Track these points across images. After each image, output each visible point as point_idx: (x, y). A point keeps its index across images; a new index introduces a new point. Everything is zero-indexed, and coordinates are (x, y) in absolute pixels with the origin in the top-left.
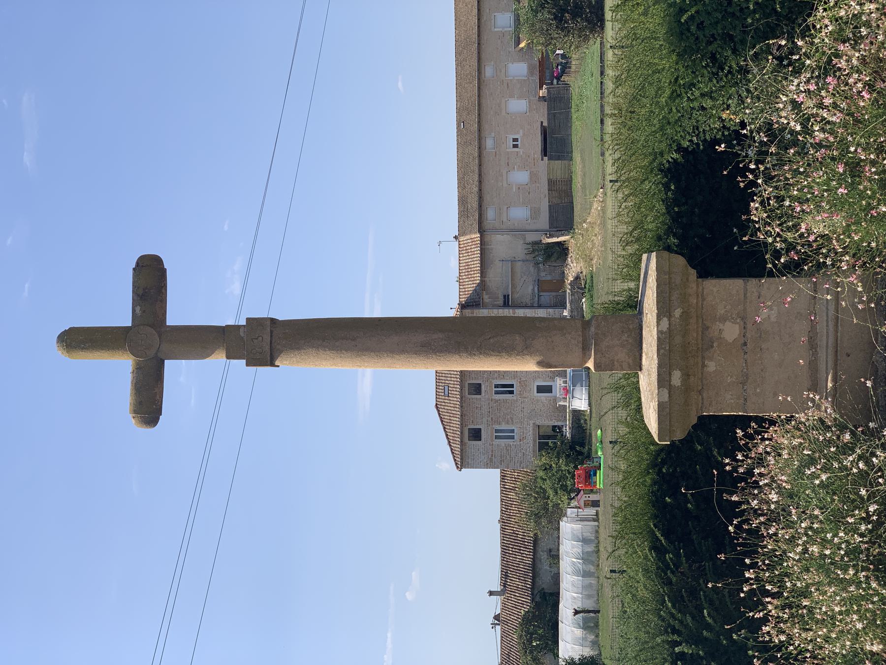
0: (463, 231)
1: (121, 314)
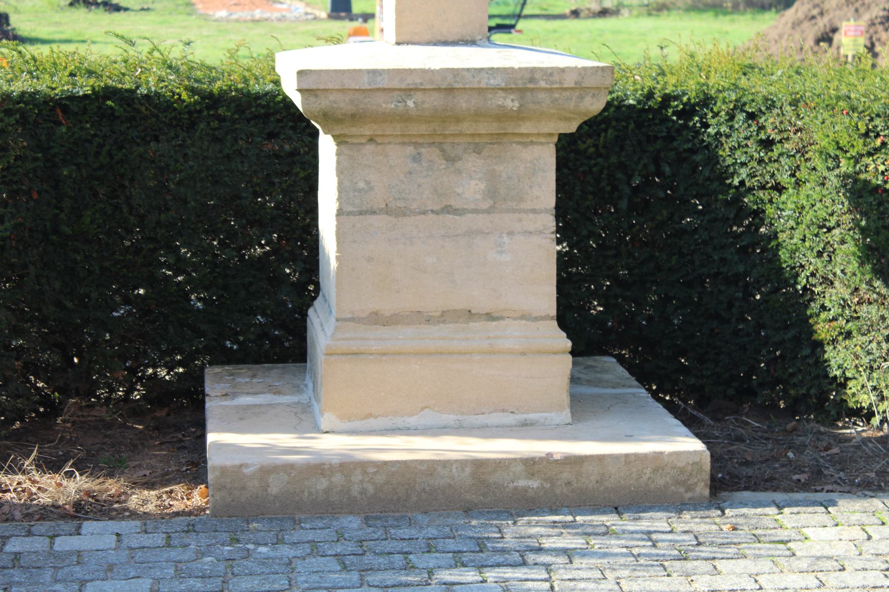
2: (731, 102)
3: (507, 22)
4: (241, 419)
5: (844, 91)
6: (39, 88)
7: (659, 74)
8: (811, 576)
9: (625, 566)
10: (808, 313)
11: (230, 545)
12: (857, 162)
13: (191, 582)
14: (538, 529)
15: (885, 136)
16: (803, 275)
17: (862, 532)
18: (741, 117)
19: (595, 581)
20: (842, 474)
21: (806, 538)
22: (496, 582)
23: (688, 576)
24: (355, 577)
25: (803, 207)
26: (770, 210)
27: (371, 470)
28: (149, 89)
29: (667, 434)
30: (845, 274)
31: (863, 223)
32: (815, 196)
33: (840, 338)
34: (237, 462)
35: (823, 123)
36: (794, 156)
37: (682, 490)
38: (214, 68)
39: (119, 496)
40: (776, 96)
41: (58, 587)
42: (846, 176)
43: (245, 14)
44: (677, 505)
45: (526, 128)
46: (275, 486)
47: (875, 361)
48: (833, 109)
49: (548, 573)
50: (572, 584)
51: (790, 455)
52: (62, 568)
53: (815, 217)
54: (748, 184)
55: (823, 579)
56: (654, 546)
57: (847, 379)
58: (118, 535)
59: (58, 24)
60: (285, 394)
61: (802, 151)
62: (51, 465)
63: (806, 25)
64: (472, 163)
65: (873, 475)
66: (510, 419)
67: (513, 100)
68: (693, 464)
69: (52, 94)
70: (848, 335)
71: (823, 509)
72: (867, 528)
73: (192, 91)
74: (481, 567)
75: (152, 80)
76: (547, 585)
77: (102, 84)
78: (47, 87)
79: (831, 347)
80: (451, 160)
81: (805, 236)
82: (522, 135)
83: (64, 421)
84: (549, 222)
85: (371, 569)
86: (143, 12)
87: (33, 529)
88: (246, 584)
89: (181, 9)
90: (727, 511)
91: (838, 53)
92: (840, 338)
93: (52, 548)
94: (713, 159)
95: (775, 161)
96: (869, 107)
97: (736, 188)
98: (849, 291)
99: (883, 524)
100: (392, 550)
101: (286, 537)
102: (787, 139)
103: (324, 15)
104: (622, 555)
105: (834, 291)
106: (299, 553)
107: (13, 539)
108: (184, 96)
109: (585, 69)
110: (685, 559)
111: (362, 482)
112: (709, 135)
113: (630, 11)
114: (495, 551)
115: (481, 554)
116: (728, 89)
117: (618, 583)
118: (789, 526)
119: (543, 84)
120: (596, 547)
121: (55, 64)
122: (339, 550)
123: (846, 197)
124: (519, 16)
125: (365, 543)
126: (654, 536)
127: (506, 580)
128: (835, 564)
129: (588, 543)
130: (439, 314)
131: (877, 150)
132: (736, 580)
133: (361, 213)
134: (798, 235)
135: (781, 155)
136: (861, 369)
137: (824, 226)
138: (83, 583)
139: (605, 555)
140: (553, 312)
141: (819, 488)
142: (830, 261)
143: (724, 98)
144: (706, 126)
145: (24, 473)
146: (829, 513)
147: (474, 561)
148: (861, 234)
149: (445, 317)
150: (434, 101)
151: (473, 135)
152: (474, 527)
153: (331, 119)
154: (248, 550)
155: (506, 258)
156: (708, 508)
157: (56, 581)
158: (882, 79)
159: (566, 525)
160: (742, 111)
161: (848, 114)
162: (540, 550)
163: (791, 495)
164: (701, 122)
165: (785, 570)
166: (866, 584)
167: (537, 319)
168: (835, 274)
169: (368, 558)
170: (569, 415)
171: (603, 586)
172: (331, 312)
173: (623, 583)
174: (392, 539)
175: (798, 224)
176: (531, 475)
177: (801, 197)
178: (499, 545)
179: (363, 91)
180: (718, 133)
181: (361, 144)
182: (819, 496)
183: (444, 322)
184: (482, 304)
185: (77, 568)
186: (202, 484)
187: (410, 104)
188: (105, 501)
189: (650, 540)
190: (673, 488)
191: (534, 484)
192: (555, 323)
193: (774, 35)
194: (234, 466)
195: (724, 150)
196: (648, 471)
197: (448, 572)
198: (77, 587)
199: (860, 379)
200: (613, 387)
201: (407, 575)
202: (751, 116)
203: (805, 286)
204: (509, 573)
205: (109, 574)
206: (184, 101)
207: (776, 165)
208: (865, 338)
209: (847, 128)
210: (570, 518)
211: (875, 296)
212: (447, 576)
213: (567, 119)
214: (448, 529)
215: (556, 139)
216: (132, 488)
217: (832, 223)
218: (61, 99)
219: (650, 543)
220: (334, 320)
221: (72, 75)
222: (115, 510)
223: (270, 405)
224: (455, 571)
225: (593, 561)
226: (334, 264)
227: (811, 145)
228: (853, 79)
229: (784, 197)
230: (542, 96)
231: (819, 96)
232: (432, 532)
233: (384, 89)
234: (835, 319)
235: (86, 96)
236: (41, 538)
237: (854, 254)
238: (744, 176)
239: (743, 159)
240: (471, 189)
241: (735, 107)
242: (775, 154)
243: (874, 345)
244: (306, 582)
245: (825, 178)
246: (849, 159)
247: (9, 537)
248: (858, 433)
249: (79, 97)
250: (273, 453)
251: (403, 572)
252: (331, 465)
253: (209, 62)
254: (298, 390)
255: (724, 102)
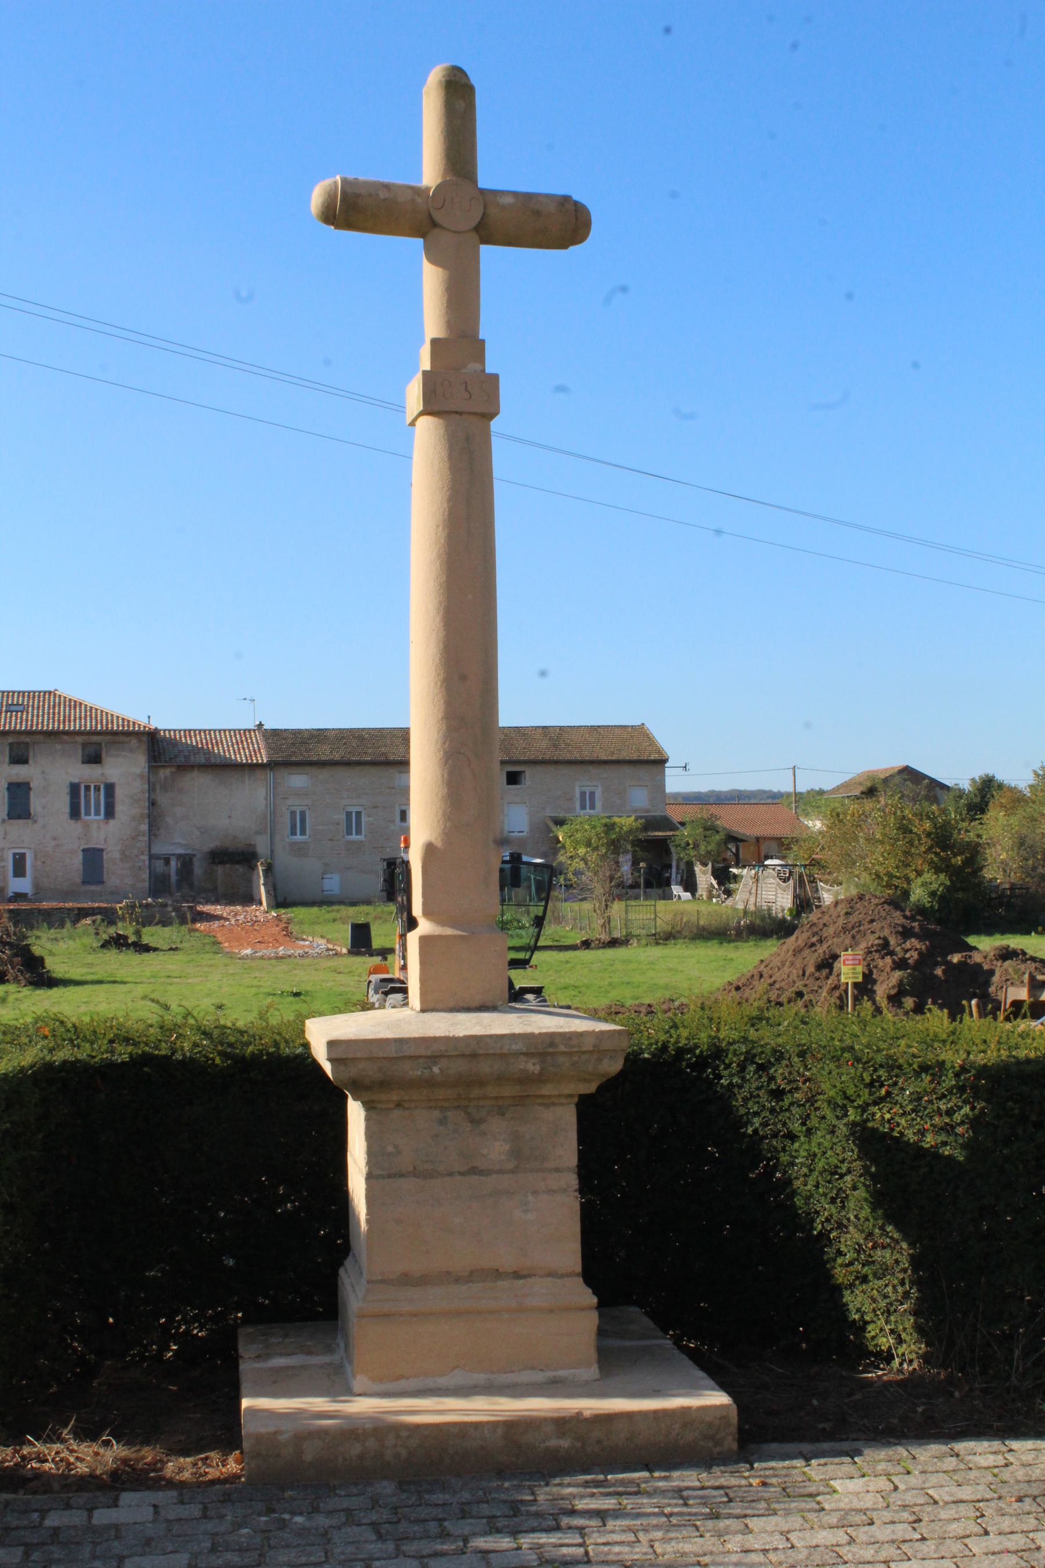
0: (274, 737)
1: (498, 171)
2: (741, 1054)
3: (521, 955)
4: (275, 1382)
5: (848, 1042)
6: (79, 1057)
7: (671, 1027)
8: (841, 1533)
9: (657, 1527)
10: (825, 1258)
11: (266, 1515)
12: (864, 1110)
13: (229, 1556)
14: (570, 1490)
15: (889, 1086)
16: (818, 1221)
17: (888, 1483)
18: (752, 1068)
19: (630, 1544)
20: (865, 1421)
21: (834, 1491)
22: (531, 1549)
23: (720, 1536)
24: (391, 1546)
25: (815, 1155)
26: (784, 1158)
27: (404, 1434)
28: (184, 1055)
29: (693, 1388)
30: (859, 1219)
31: (873, 1169)
32: (826, 1144)
33: (857, 1282)
34: (271, 1429)
35: (830, 1073)
36: (803, 1105)
37: (711, 1444)
38: (246, 1032)
39: (155, 1464)
40: (784, 1047)
41: (97, 1563)
42: (854, 1124)
43: (269, 952)
44: (706, 1461)
45: (547, 1090)
46: (310, 1453)
47: (891, 1304)
48: (839, 1060)
49: (583, 1537)
50: (606, 1549)
51: (815, 1402)
52: (100, 1543)
53: (828, 1164)
54: (761, 1133)
55: (854, 1534)
56: (686, 1505)
57: (867, 1323)
58: (155, 1506)
59: (90, 965)
60: (317, 1355)
61: (811, 1100)
62: (88, 1433)
63: (806, 952)
64: (496, 1125)
65: (895, 1421)
66: (540, 1377)
67: (534, 1064)
68: (720, 1419)
69: (92, 1061)
70: (864, 1279)
71: (848, 1459)
72: (893, 1478)
73: (223, 1054)
74: (515, 1533)
75: (186, 1046)
76: (581, 1550)
77: (140, 1052)
78: (89, 1056)
79: (849, 1292)
80: (475, 1122)
81: (818, 1183)
82: (543, 1096)
83: (100, 1384)
84: (572, 1180)
85: (407, 1538)
86: (172, 952)
87: (71, 1501)
88: (284, 1557)
89: (208, 948)
90: (756, 1465)
91: (839, 980)
92: (857, 1282)
93: (90, 1522)
94: (727, 1109)
95: (787, 1110)
96: (872, 1059)
97: (750, 1136)
98: (864, 1236)
99: (908, 1473)
100: (427, 1517)
101: (321, 1505)
102: (797, 1089)
103: (344, 951)
104: (654, 1514)
105: (849, 1236)
106: (334, 1522)
107: (52, 1513)
108: (218, 1061)
109: (602, 1032)
110: (717, 1518)
111: (395, 1446)
112: (722, 1085)
113: (639, 940)
114: (529, 1514)
115: (515, 1519)
116: (738, 1042)
117: (652, 1546)
118: (817, 1479)
119: (562, 1048)
120: (629, 1507)
121: (95, 1032)
122: (374, 1518)
123: (855, 1145)
124: (534, 948)
125: (400, 1510)
126: (685, 1493)
127: (541, 1546)
128: (864, 1517)
129: (620, 1504)
130: (467, 1274)
131: (882, 1099)
132: (768, 1539)
133: (390, 1176)
134: (811, 1182)
135: (792, 1104)
136: (878, 1312)
137: (836, 1173)
138: (121, 1559)
139: (638, 1516)
140: (579, 1268)
141: (844, 1437)
142: (843, 1207)
143: (735, 1050)
144: (720, 1077)
145: (63, 1441)
146: (856, 1463)
147: (509, 1526)
148: (871, 1180)
149: (475, 1275)
150: (459, 1067)
151: (496, 1098)
152: (507, 1489)
153: (360, 1088)
154: (284, 1520)
155: (530, 1216)
156: (737, 1462)
157: (95, 1557)
158: (883, 1029)
159: (598, 1484)
160: (753, 1062)
161: (852, 1064)
162: (573, 1512)
163: (817, 1445)
164: (713, 1073)
165: (815, 1526)
166: (895, 1537)
167: (562, 1276)
168: (848, 1219)
169: (403, 1527)
170: (597, 1370)
171: (637, 1550)
172: (361, 1273)
173: (657, 1545)
174: (427, 1505)
175: (811, 1171)
176: (562, 1435)
177: (813, 1144)
178: (533, 1508)
179: (391, 1059)
180: (731, 1084)
181: (388, 1109)
182: (845, 1446)
183: (472, 1281)
184: (508, 1261)
185: (116, 1544)
186: (236, 1449)
187: (436, 1070)
188: (142, 1470)
189: (682, 1497)
190: (702, 1443)
191: (565, 1443)
192: (581, 1279)
193: (776, 962)
194: (268, 1433)
195: (737, 1100)
196: (677, 1426)
197: (482, 1539)
198: (115, 1564)
199: (879, 1322)
200: (640, 1339)
201: (442, 1543)
202: (762, 1068)
203: (821, 1231)
204: (543, 1539)
205: (147, 1549)
206: (217, 1065)
207: (787, 1114)
208: (880, 1283)
209: (853, 1078)
210: (601, 1477)
211: (888, 1240)
212: (482, 1543)
213: (586, 1080)
214: (481, 1493)
215: (576, 1100)
216: (167, 1455)
217: (844, 1170)
218: (100, 1066)
219: (681, 1502)
220: (365, 1283)
221: (111, 1042)
222: (152, 1478)
223: (302, 1367)
224: (489, 1538)
225: (627, 1522)
226: (363, 1225)
227: (820, 1094)
228: (856, 1029)
229: (796, 1145)
230: (561, 1059)
231: (825, 1047)
232: (466, 1496)
233: (411, 1057)
234: (851, 1264)
235: (123, 1063)
236: (79, 1512)
237: (866, 1200)
238: (757, 1125)
239: (756, 1109)
240: (496, 1150)
241: (746, 1059)
242: (786, 1102)
243: (890, 1289)
244: (342, 1553)
245: (834, 1126)
246: (857, 1108)
247: (49, 1510)
248: (878, 1376)
249: (117, 1064)
250: (306, 1419)
251: (438, 1541)
252: (364, 1430)
253: (240, 1024)
254: (329, 1349)
255: (735, 1054)
